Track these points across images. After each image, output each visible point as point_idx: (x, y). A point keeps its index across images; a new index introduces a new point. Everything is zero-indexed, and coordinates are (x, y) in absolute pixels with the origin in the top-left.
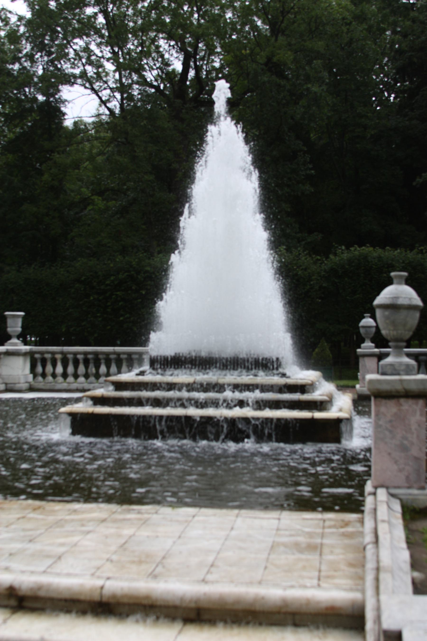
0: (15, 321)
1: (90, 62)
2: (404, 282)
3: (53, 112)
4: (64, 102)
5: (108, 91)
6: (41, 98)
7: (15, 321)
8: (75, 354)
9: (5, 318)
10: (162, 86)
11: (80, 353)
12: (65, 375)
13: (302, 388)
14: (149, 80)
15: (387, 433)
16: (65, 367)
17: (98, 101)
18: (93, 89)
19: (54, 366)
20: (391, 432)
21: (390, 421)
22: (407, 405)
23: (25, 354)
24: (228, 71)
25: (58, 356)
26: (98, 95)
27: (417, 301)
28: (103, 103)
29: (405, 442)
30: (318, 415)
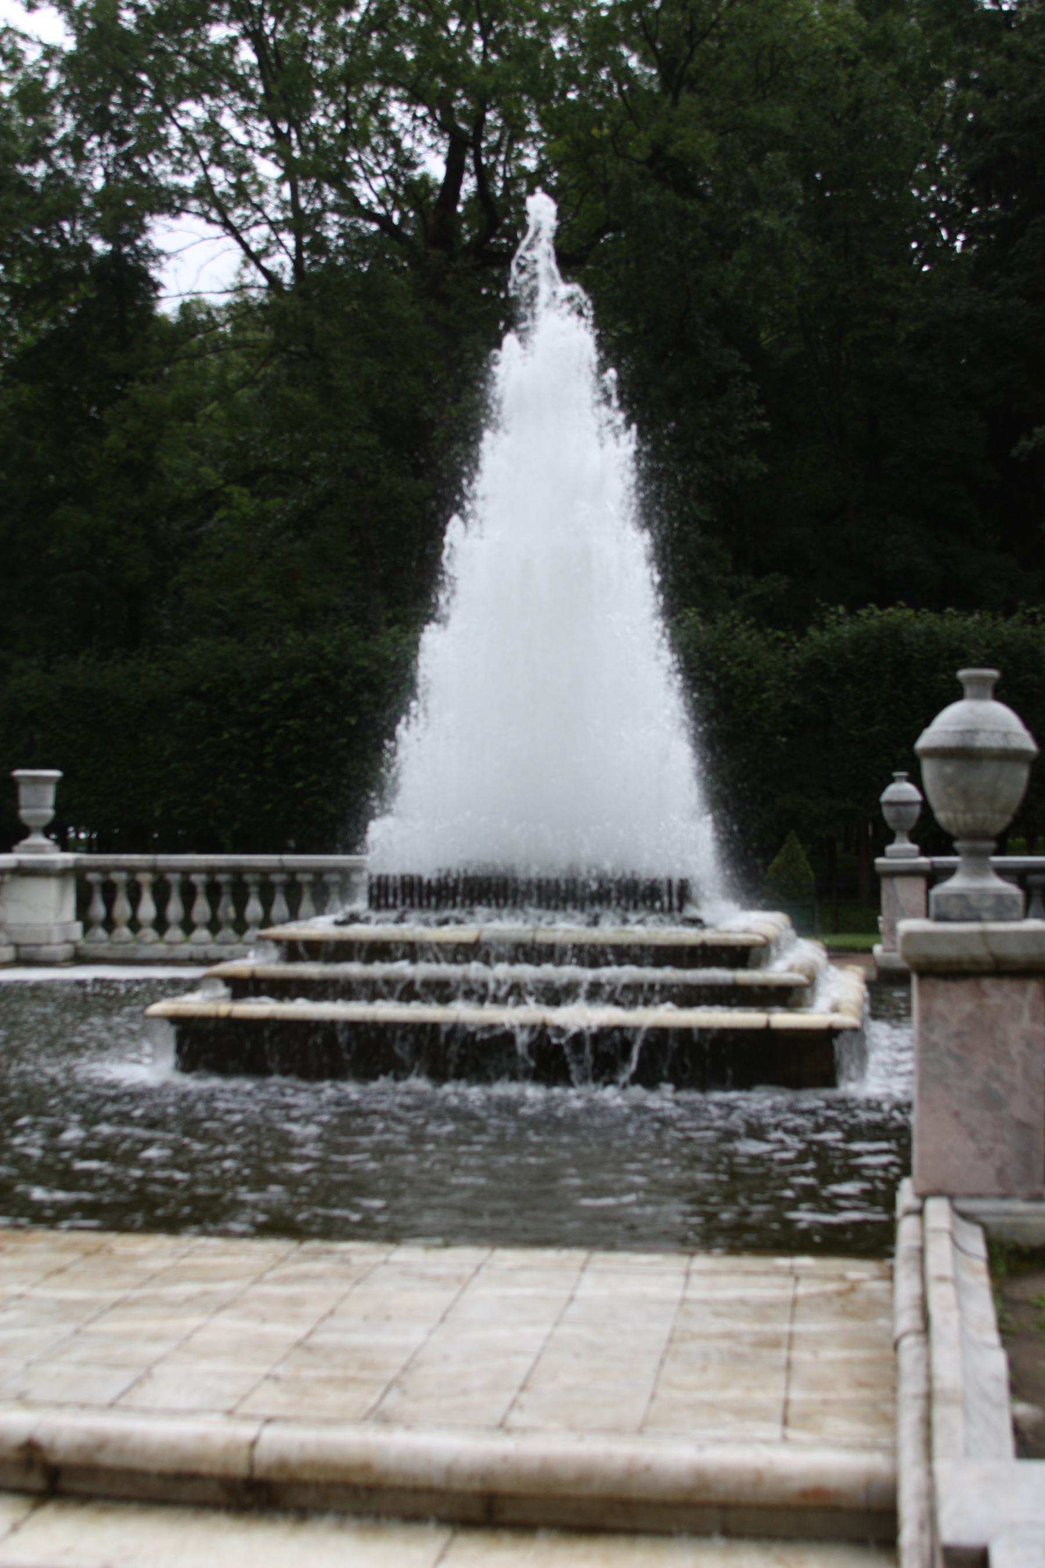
0: (39, 791)
1: (219, 159)
2: (989, 693)
3: (129, 280)
4: (156, 255)
5: (265, 230)
6: (100, 246)
7: (39, 791)
8: (186, 872)
9: (13, 785)
10: (396, 217)
11: (197, 870)
12: (161, 924)
13: (740, 955)
14: (363, 201)
15: (951, 1063)
16: (161, 903)
17: (239, 253)
18: (227, 225)
19: (135, 901)
20: (959, 1060)
21: (959, 1034)
22: (999, 995)
23: (63, 873)
24: (556, 178)
25: (145, 878)
26: (239, 240)
27: (1024, 740)
28: (253, 257)
29: (995, 1085)
30: (782, 1019)
